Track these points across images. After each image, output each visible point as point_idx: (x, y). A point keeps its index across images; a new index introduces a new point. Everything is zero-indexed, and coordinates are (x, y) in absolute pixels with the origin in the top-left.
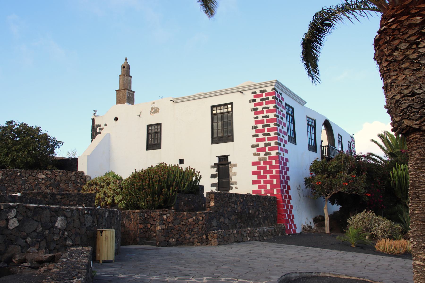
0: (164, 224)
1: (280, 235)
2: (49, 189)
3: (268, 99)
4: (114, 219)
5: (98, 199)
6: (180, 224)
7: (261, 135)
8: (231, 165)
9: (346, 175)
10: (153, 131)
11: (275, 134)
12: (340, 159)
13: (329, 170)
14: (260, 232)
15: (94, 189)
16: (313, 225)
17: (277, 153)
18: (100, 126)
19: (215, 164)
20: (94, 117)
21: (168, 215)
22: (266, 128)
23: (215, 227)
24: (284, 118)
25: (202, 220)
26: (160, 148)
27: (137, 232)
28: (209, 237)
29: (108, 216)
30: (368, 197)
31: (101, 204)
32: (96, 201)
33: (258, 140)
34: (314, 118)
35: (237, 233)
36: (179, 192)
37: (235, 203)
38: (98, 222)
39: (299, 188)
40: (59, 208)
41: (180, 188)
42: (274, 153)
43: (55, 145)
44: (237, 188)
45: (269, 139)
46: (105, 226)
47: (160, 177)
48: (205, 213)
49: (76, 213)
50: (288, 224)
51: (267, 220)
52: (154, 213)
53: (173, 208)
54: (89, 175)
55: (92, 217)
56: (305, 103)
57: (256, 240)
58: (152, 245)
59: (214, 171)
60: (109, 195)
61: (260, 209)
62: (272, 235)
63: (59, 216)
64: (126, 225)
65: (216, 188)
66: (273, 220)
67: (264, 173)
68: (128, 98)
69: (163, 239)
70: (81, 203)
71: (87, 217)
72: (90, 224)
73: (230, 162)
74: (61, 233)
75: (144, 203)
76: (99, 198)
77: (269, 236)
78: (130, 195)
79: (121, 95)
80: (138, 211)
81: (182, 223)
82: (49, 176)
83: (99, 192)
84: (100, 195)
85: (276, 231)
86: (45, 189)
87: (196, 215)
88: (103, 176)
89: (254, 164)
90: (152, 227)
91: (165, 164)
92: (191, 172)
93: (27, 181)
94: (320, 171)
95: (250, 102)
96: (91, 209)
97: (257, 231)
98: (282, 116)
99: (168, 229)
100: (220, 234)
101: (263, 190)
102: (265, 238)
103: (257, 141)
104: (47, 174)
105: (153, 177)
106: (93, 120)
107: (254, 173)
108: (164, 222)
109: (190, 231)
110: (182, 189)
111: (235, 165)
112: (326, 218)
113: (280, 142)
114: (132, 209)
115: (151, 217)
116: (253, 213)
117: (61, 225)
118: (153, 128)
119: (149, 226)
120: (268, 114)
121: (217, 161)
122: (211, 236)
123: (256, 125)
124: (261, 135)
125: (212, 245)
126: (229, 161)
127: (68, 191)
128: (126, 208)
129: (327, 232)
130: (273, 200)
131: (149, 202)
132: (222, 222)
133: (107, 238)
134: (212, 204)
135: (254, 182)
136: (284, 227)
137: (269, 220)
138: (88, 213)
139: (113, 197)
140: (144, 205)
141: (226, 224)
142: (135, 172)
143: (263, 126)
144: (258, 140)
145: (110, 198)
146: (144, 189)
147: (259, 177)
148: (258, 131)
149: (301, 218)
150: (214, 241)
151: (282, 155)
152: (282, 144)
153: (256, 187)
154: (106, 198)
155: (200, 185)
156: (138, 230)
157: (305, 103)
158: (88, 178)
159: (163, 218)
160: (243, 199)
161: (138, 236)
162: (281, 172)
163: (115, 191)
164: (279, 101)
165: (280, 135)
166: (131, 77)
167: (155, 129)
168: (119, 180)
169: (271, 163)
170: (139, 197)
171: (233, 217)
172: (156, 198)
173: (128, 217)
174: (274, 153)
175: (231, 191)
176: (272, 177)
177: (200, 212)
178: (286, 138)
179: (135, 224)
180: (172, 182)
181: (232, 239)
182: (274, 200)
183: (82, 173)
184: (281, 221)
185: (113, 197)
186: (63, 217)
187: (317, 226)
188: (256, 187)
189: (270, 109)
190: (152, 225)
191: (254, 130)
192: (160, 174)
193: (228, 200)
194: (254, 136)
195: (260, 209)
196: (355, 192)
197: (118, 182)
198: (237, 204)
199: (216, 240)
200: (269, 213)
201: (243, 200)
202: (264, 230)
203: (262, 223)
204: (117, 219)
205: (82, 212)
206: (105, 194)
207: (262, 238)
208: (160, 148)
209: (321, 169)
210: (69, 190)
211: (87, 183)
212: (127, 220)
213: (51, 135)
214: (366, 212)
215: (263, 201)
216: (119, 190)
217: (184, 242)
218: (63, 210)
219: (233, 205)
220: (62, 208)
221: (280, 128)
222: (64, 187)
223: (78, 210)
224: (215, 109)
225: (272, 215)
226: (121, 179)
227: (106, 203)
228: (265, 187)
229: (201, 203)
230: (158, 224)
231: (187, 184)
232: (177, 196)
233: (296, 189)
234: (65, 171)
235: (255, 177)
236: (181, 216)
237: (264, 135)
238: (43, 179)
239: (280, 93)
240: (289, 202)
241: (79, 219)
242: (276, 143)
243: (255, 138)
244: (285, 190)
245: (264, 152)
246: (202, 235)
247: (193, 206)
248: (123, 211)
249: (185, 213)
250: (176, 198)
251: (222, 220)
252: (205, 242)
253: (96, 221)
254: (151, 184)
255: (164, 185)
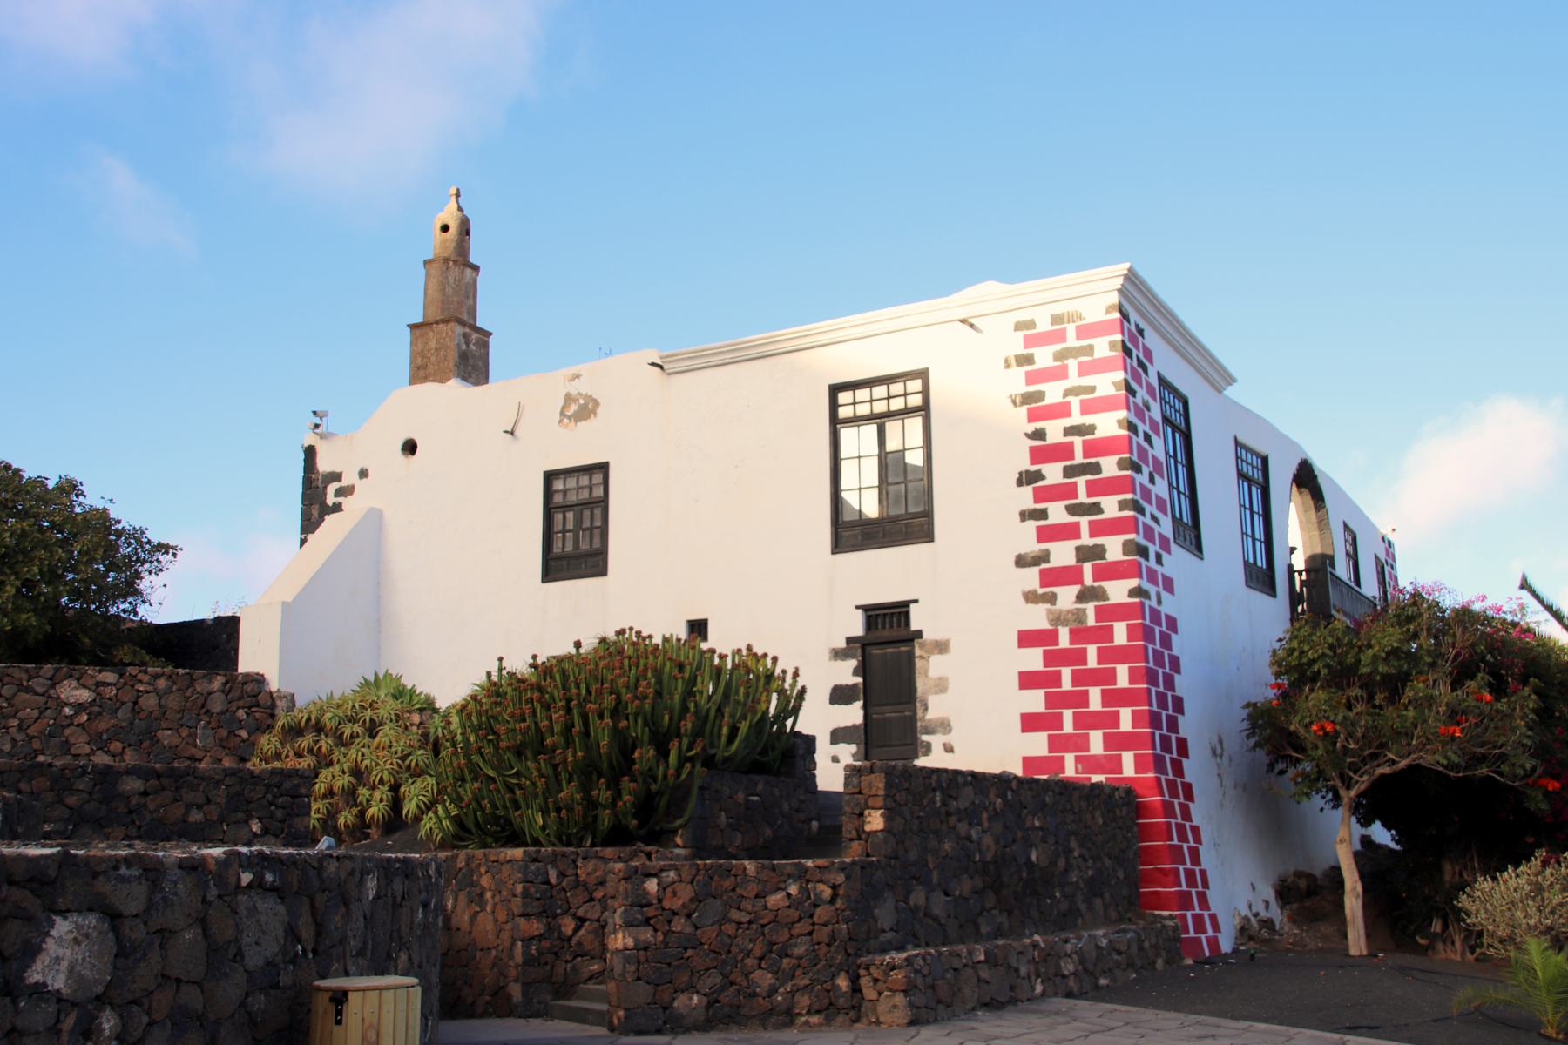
0: (647, 922)
1: (1160, 963)
2: (108, 752)
3: (1089, 350)
4: (413, 912)
5: (325, 797)
6: (725, 919)
7: (1057, 513)
8: (922, 646)
9: (1443, 692)
10: (573, 498)
11: (1122, 505)
12: (1410, 619)
13: (1365, 670)
14: (1080, 953)
15: (310, 750)
16: (1276, 914)
17: (1133, 592)
18: (337, 477)
19: (850, 640)
20: (310, 439)
21: (668, 875)
22: (1081, 482)
23: (889, 935)
24: (1154, 438)
25: (832, 901)
26: (601, 571)
27: (511, 957)
28: (865, 982)
29: (377, 897)
30: (1547, 794)
31: (341, 821)
32: (314, 807)
33: (1049, 534)
34: (1263, 450)
35: (991, 960)
36: (709, 762)
37: (971, 816)
38: (318, 934)
39: (1219, 751)
40: (65, 859)
41: (712, 745)
42: (1118, 591)
43: (143, 562)
44: (949, 749)
45: (1097, 529)
46: (361, 953)
47: (619, 697)
48: (843, 868)
49: (182, 889)
50: (1189, 913)
51: (1101, 895)
52: (591, 866)
53: (678, 840)
54: (288, 689)
55: (281, 909)
56: (1231, 380)
57: (1069, 995)
58: (583, 1021)
59: (846, 673)
60: (375, 776)
61: (1073, 844)
62: (1131, 965)
63: (64, 913)
64: (454, 922)
65: (853, 748)
66: (1125, 892)
67: (1075, 682)
68: (464, 357)
69: (643, 993)
70: (240, 815)
71: (253, 911)
72: (271, 949)
73: (919, 634)
74: (69, 1022)
75: (545, 812)
76: (330, 793)
77: (1118, 973)
78: (475, 779)
79: (433, 344)
80: (518, 853)
81: (734, 914)
82: (111, 692)
83: (330, 764)
84: (335, 777)
85: (1146, 945)
86: (87, 749)
87: (802, 875)
88: (348, 692)
89: (1027, 639)
90: (582, 932)
91: (639, 633)
92: (754, 677)
93: (6, 717)
94: (1324, 672)
95: (1008, 366)
96: (279, 859)
97: (1069, 947)
98: (1147, 429)
99: (666, 945)
100: (917, 972)
101: (1070, 759)
102: (1103, 982)
103: (1040, 540)
104: (98, 684)
105: (589, 692)
106: (310, 452)
107: (1028, 680)
108: (650, 912)
109: (775, 952)
110: (721, 753)
111: (942, 647)
112: (1348, 885)
113: (1144, 542)
114: (485, 846)
115: (577, 883)
116: (1044, 863)
117: (71, 970)
118: (571, 483)
119: (568, 925)
120: (1088, 420)
121: (857, 628)
122: (876, 980)
123: (1034, 468)
124: (1057, 513)
125: (878, 1023)
126: (914, 627)
127: (192, 758)
128: (456, 837)
129: (1353, 951)
130: (1118, 803)
131: (570, 810)
132: (917, 908)
133: (372, 1035)
134: (875, 821)
135: (1030, 723)
136: (1175, 929)
137: (1107, 895)
138: (258, 884)
139: (395, 788)
140: (544, 828)
141: (936, 919)
142: (500, 669)
143: (1069, 472)
144: (1049, 534)
145: (382, 793)
146: (541, 748)
147: (1051, 701)
148: (1044, 495)
149: (1234, 888)
150: (893, 1006)
151: (1154, 603)
152: (1153, 549)
153: (1038, 745)
154: (363, 792)
155: (799, 734)
156: (513, 944)
157: (1231, 380)
158: (281, 704)
159: (646, 892)
160: (1003, 797)
161: (513, 973)
162: (1151, 677)
163: (403, 758)
164: (1135, 363)
165: (1141, 511)
166: (476, 268)
167: (579, 488)
168: (421, 710)
169: (1108, 633)
170: (521, 787)
171: (965, 886)
172: (602, 794)
173: (467, 881)
174: (1118, 591)
175: (922, 762)
176: (1114, 698)
177: (821, 862)
178: (1166, 527)
179: (502, 917)
180: (676, 714)
181: (970, 992)
182: (1128, 804)
183: (259, 680)
184: (1159, 901)
185: (395, 788)
186: (92, 920)
187: (1292, 919)
188: (1038, 745)
189: (1097, 394)
190: (582, 920)
191: (1028, 490)
192: (621, 681)
193: (944, 804)
194: (1025, 515)
195: (1073, 844)
196: (1483, 771)
197: (416, 718)
198: (980, 824)
199: (900, 999)
200: (1107, 861)
201: (1005, 802)
202: (1098, 947)
203: (1083, 907)
204: (425, 905)
205: (220, 879)
206: (358, 773)
207: (1092, 982)
208: (601, 571)
209: (1327, 666)
210: (199, 754)
211: (280, 723)
212: (462, 896)
213: (126, 515)
214: (1545, 864)
215: (1084, 804)
216: (420, 756)
217: (744, 1011)
218: (93, 870)
219: (963, 828)
220: (87, 860)
221: (1142, 478)
222: (176, 741)
223: (194, 867)
224: (844, 397)
225: (1121, 874)
226: (429, 707)
227: (362, 814)
228: (1079, 743)
229: (802, 816)
230: (618, 918)
231: (744, 727)
232: (697, 782)
233: (1209, 752)
234: (181, 671)
235: (1035, 701)
236: (728, 883)
237: (1072, 510)
238: (79, 707)
239: (1137, 326)
240: (1187, 815)
241: (203, 922)
242: (1128, 547)
243: (1032, 525)
244: (1168, 756)
245: (1076, 589)
246: (833, 977)
247: (768, 832)
248: (442, 855)
249: (750, 866)
250: (695, 791)
251: (918, 897)
252: (846, 1010)
253: (307, 932)
254: (578, 727)
255: (638, 730)
